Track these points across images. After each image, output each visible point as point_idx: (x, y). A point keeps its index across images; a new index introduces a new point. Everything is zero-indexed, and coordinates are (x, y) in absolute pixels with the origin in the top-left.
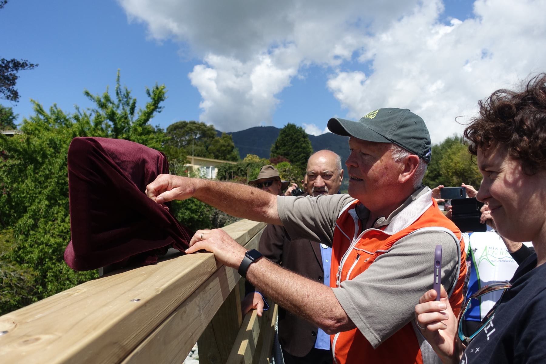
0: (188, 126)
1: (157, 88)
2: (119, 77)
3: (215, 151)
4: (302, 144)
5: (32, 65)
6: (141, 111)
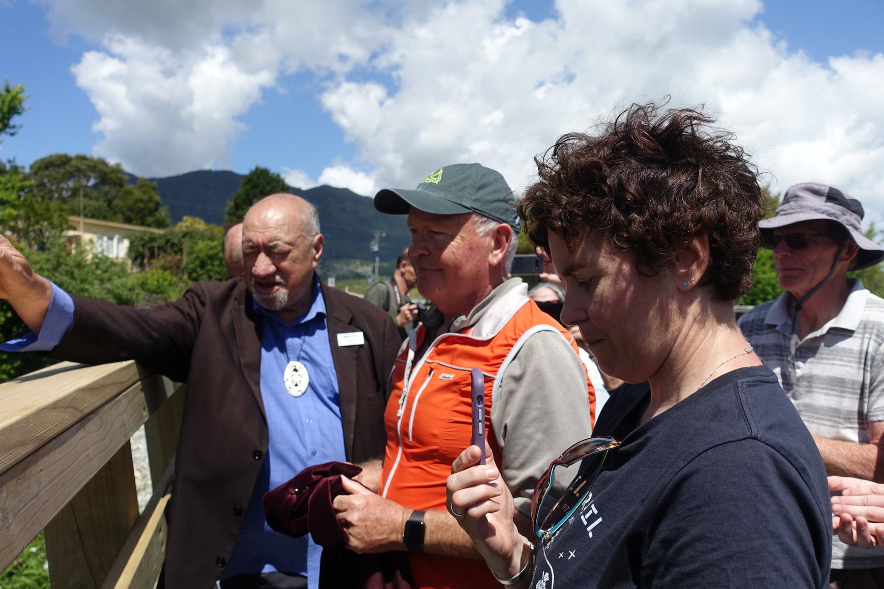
0: (73, 163)
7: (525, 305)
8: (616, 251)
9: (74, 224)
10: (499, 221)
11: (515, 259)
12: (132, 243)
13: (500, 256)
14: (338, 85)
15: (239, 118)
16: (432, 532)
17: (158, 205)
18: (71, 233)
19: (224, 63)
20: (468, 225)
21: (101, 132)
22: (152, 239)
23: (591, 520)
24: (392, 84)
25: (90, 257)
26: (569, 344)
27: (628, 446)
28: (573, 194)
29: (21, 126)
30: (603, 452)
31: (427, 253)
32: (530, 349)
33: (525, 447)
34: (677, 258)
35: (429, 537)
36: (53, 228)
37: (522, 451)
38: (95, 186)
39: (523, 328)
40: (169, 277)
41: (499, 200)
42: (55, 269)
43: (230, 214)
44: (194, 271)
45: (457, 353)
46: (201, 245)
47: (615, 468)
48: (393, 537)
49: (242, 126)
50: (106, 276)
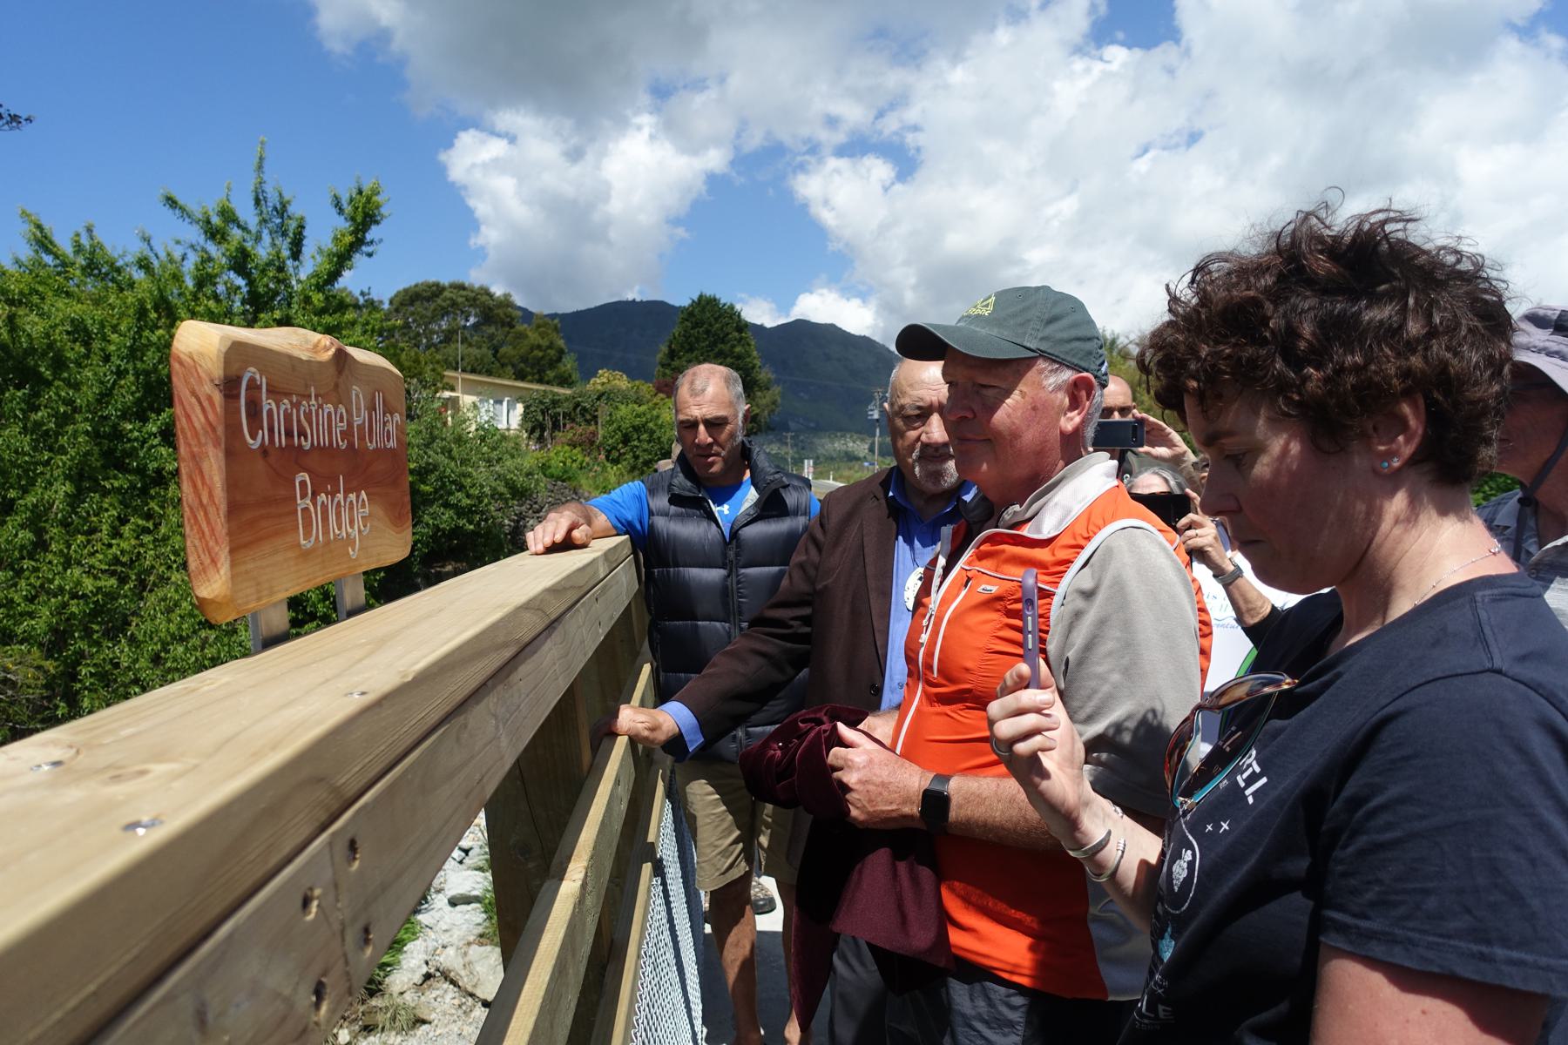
0: (446, 294)
1: (360, 192)
2: (261, 158)
3: (515, 361)
4: (733, 346)
5: (14, 118)
6: (320, 251)
7: (1108, 492)
8: (1277, 422)
9: (451, 382)
10: (1076, 368)
11: (1100, 424)
12: (526, 408)
13: (1078, 419)
14: (821, 161)
15: (675, 221)
16: (960, 807)
17: (561, 352)
18: (447, 394)
19: (652, 137)
20: (1031, 375)
21: (482, 248)
22: (555, 403)
23: (1250, 781)
24: (905, 162)
25: (473, 428)
26: (1171, 548)
27: (1309, 686)
28: (1217, 343)
29: (381, 240)
30: (1271, 695)
31: (970, 415)
32: (1109, 552)
33: (1095, 692)
34: (1375, 429)
35: (953, 814)
36: (425, 387)
37: (1089, 698)
38: (476, 326)
39: (1100, 522)
40: (580, 457)
41: (1078, 339)
42: (427, 446)
43: (663, 366)
44: (614, 448)
45: (1003, 556)
46: (624, 410)
47: (1288, 717)
48: (907, 810)
49: (681, 232)
50: (494, 455)
